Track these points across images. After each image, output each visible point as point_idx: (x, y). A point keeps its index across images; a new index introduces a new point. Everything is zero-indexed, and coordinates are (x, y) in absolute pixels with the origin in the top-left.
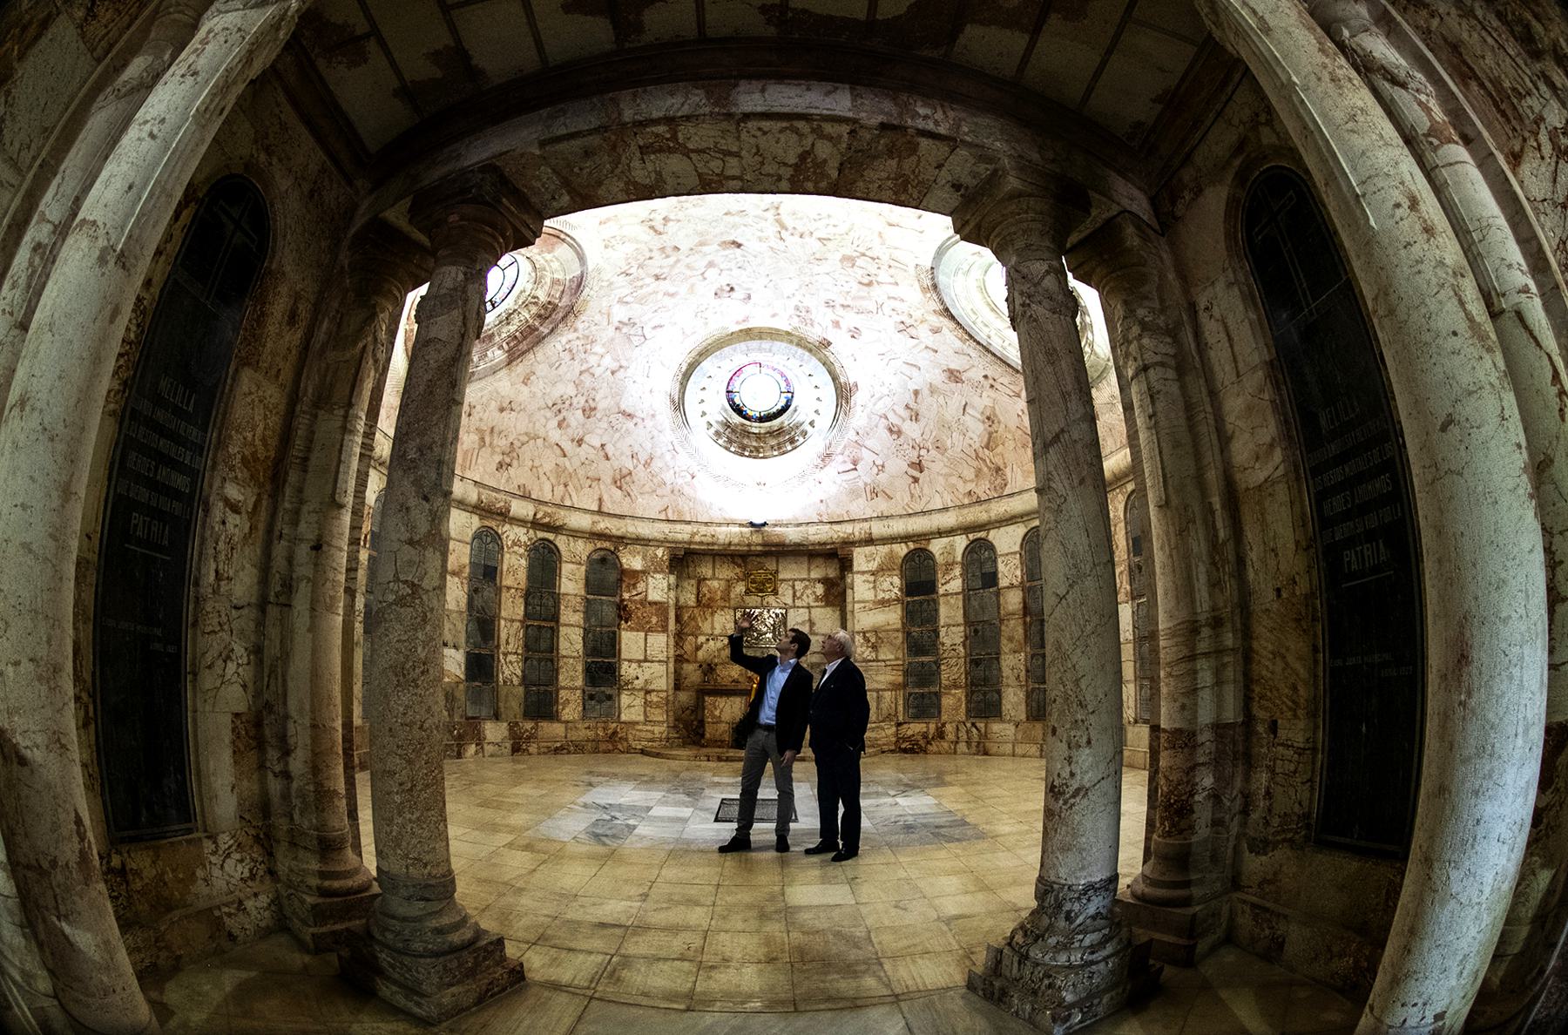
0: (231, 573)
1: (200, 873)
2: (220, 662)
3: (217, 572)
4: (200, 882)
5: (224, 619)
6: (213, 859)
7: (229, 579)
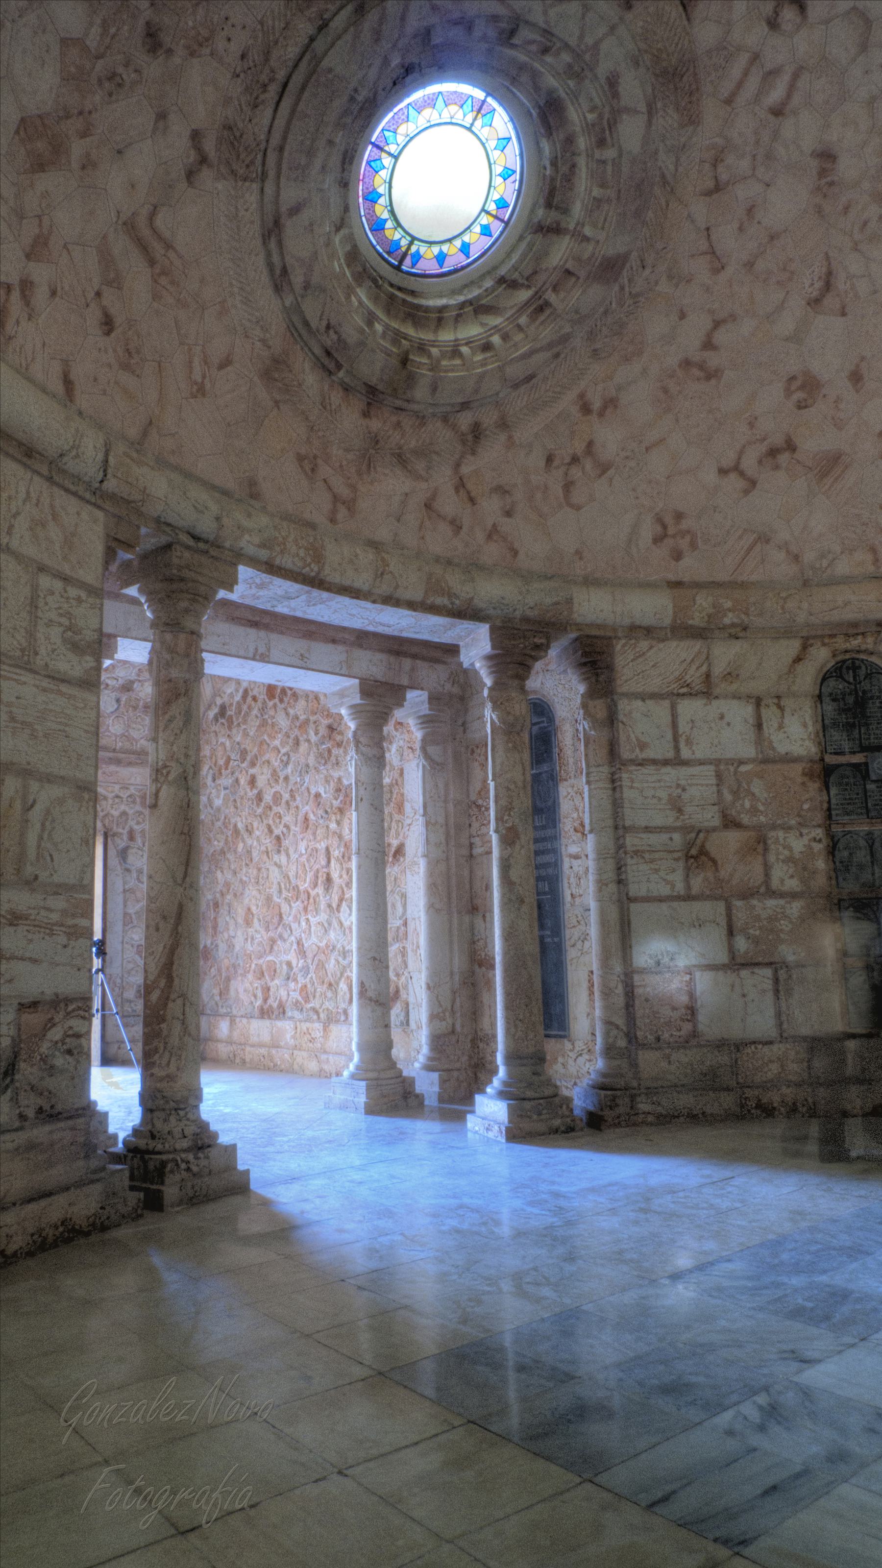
0: (581, 892)
1: (560, 1060)
2: (580, 942)
3: (572, 895)
4: (559, 1064)
5: (580, 918)
6: (571, 1054)
7: (581, 896)
